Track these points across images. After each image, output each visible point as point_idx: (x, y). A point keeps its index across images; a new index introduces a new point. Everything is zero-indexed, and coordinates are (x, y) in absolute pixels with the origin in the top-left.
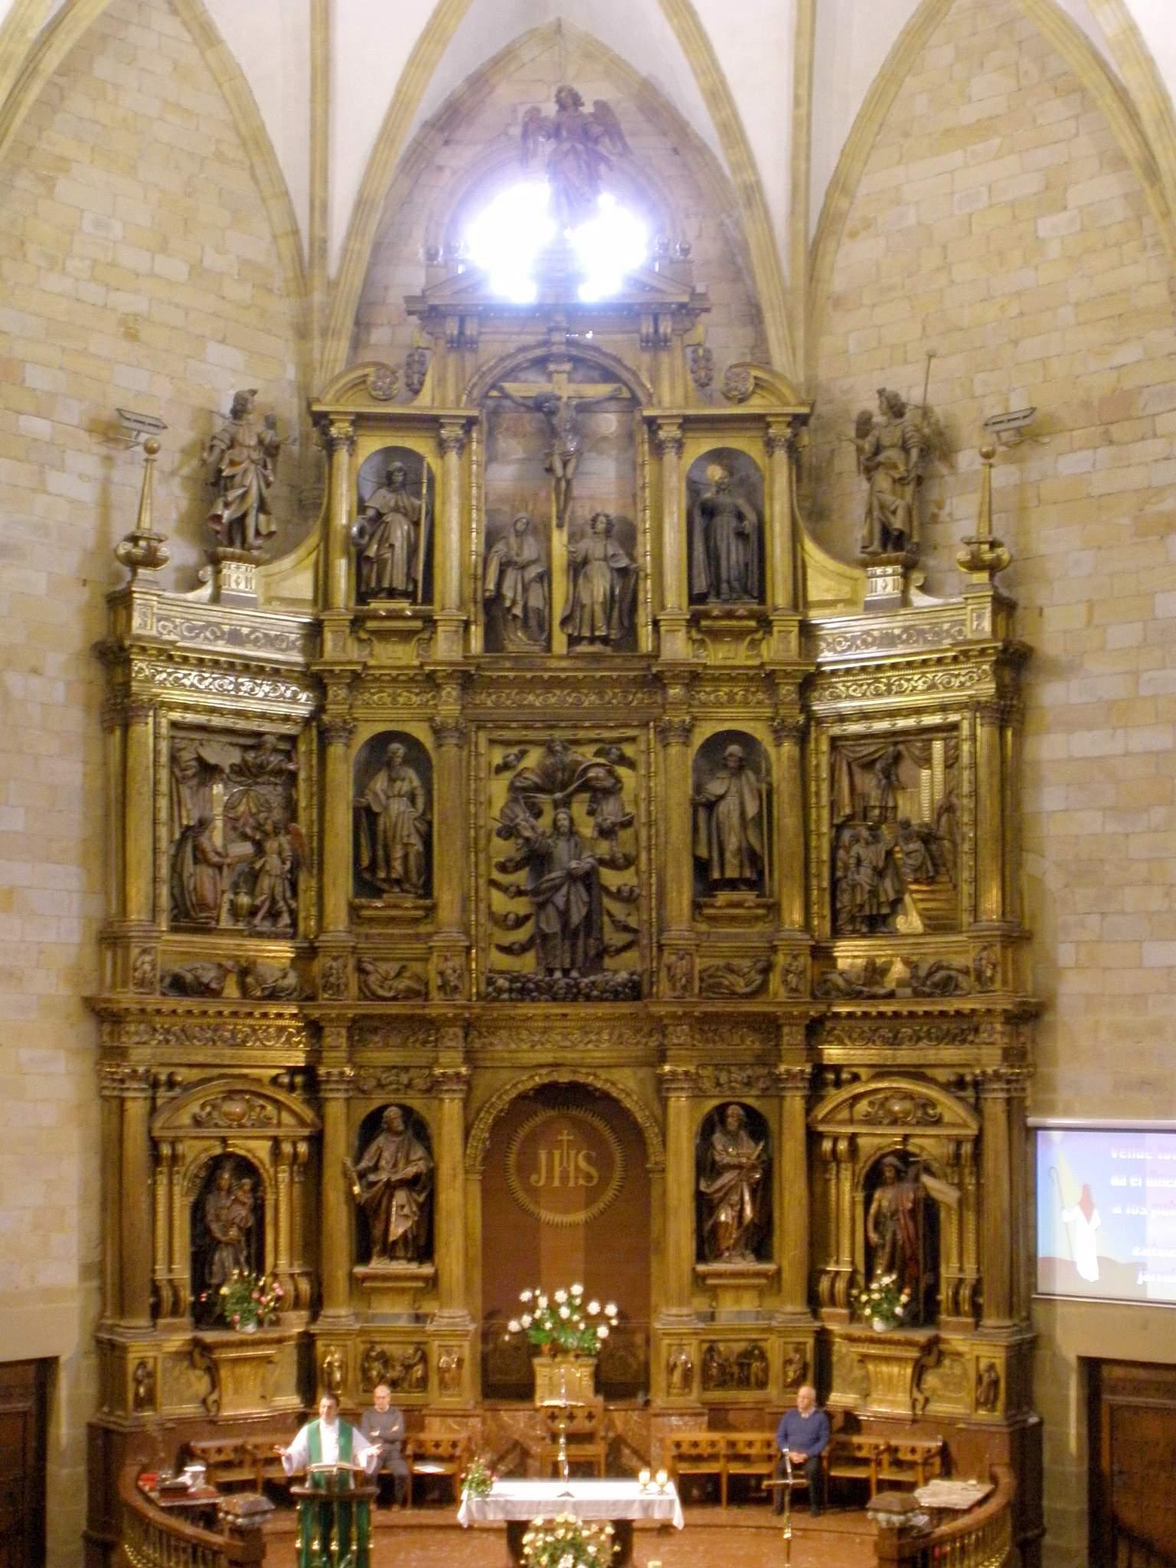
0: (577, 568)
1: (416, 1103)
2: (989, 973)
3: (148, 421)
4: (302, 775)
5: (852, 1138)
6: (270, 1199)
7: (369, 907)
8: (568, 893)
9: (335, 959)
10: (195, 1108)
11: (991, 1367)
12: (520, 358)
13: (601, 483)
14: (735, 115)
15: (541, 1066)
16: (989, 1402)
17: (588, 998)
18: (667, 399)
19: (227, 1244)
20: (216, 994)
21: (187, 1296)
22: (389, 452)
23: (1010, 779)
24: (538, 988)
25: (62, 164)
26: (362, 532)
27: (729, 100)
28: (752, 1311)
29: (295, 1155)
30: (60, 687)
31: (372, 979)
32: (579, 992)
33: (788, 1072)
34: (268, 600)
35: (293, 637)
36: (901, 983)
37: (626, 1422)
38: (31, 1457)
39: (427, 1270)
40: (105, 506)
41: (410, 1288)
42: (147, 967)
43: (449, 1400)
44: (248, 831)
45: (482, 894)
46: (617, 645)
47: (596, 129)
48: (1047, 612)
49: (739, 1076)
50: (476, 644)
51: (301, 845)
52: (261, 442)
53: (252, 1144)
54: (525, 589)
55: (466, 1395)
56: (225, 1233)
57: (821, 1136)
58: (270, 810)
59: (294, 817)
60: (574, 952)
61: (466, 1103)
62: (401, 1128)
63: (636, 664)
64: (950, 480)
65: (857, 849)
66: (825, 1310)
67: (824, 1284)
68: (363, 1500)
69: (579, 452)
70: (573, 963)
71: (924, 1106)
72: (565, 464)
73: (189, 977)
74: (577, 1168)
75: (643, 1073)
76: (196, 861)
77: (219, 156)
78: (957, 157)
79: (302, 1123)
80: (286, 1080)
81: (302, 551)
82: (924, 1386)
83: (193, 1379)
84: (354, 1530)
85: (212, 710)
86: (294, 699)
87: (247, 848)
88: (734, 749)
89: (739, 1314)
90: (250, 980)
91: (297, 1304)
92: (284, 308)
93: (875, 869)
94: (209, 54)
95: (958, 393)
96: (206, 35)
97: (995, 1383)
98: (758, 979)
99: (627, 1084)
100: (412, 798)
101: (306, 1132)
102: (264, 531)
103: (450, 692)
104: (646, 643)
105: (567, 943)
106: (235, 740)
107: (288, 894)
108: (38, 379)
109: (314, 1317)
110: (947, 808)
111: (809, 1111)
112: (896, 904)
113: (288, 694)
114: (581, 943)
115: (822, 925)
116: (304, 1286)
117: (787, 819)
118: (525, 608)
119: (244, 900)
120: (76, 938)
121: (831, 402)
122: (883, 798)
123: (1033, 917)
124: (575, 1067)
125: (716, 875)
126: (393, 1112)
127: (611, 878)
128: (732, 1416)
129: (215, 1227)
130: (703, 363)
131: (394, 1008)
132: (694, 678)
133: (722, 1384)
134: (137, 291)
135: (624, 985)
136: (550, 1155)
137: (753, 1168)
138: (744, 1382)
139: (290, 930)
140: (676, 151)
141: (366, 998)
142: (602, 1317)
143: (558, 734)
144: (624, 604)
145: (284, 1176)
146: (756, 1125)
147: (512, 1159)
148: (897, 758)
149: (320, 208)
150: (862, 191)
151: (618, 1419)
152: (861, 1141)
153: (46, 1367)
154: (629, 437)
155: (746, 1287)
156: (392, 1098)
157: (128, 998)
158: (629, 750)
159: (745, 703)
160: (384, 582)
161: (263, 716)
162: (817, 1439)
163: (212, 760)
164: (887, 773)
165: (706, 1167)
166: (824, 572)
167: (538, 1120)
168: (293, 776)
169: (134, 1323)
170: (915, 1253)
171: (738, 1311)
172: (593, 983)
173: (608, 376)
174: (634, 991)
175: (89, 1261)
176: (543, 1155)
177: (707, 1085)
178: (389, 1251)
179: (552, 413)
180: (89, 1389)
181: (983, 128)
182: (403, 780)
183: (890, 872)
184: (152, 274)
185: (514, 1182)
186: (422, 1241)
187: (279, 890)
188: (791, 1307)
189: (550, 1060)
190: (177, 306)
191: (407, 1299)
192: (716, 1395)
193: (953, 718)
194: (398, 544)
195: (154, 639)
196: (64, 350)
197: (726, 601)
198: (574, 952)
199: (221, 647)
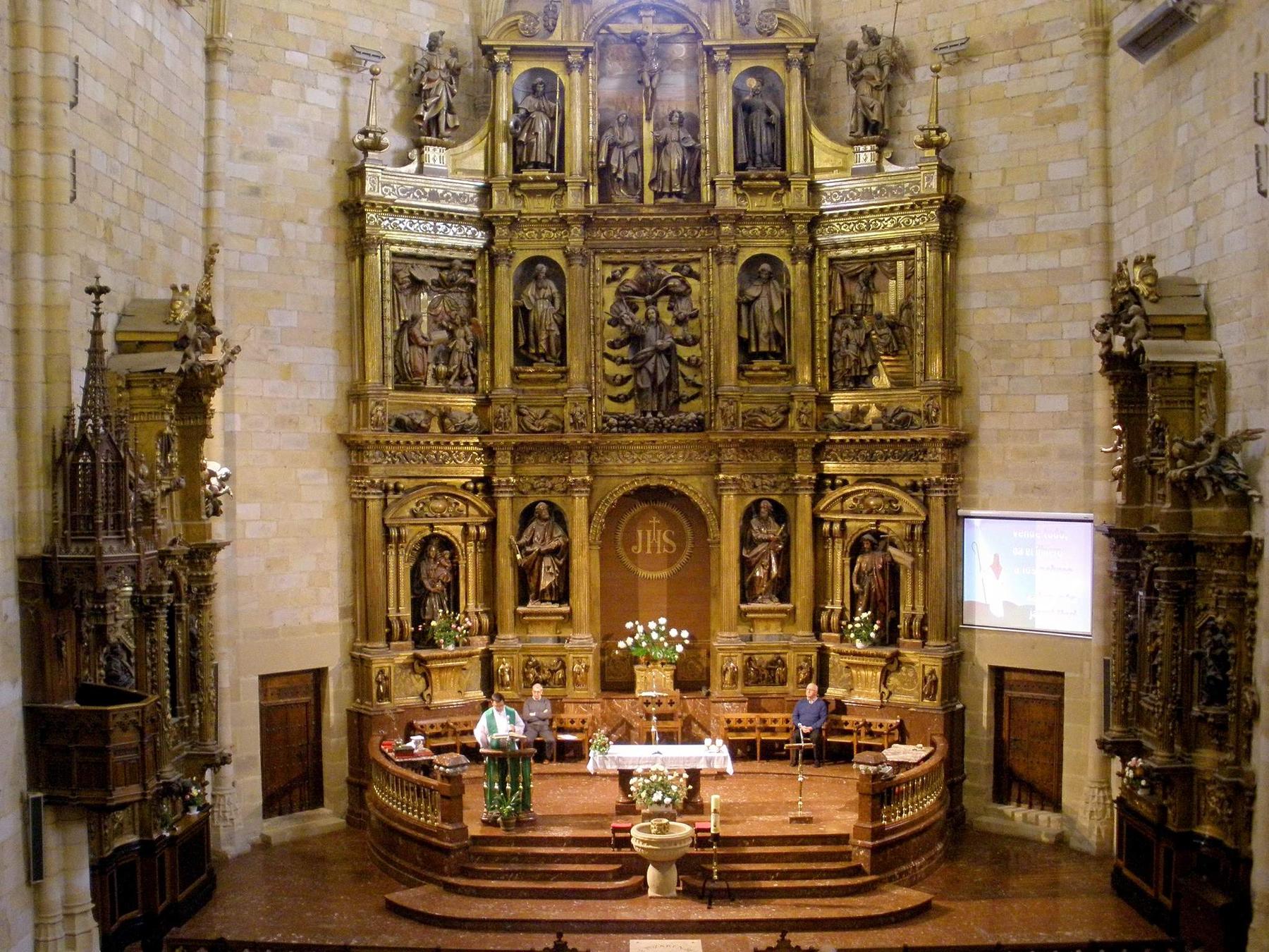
1: (557, 500)
6: (462, 563)
13: (675, 90)
15: (638, 475)
16: (930, 695)
17: (669, 430)
20: (425, 430)
22: (534, 72)
23: (948, 286)
24: (636, 424)
29: (478, 534)
30: (319, 231)
31: (526, 419)
35: (471, 195)
36: (875, 421)
37: (695, 707)
38: (312, 734)
39: (565, 609)
40: (345, 111)
42: (380, 414)
43: (580, 693)
50: (594, 198)
52: (448, 66)
53: (450, 528)
56: (434, 587)
57: (822, 521)
59: (474, 314)
60: (659, 400)
61: (590, 499)
67: (824, 617)
70: (659, 407)
72: (651, 80)
73: (407, 419)
75: (710, 478)
76: (411, 344)
79: (482, 514)
86: (473, 237)
90: (447, 421)
97: (935, 683)
98: (781, 418)
99: (695, 487)
101: (485, 520)
102: (451, 125)
103: (577, 229)
104: (706, 196)
106: (434, 263)
108: (296, 26)
109: (492, 641)
110: (907, 306)
113: (469, 233)
114: (664, 396)
115: (823, 383)
117: (800, 312)
118: (626, 175)
119: (442, 368)
120: (333, 396)
124: (660, 476)
125: (753, 349)
126: (542, 506)
132: (738, 219)
133: (757, 683)
135: (693, 421)
137: (777, 541)
138: (771, 681)
141: (523, 432)
142: (679, 639)
143: (648, 257)
146: (780, 514)
147: (620, 536)
152: (848, 524)
153: (319, 675)
154: (694, 60)
155: (773, 619)
156: (541, 497)
157: (368, 434)
159: (773, 236)
160: (531, 157)
162: (819, 718)
163: (420, 278)
165: (747, 541)
167: (638, 510)
168: (473, 287)
170: (883, 600)
171: (767, 636)
173: (680, 19)
174: (699, 425)
176: (640, 533)
178: (540, 597)
179: (642, 44)
180: (348, 688)
185: (621, 550)
191: (552, 628)
192: (754, 689)
195: (379, 198)
197: (759, 169)
198: (659, 400)
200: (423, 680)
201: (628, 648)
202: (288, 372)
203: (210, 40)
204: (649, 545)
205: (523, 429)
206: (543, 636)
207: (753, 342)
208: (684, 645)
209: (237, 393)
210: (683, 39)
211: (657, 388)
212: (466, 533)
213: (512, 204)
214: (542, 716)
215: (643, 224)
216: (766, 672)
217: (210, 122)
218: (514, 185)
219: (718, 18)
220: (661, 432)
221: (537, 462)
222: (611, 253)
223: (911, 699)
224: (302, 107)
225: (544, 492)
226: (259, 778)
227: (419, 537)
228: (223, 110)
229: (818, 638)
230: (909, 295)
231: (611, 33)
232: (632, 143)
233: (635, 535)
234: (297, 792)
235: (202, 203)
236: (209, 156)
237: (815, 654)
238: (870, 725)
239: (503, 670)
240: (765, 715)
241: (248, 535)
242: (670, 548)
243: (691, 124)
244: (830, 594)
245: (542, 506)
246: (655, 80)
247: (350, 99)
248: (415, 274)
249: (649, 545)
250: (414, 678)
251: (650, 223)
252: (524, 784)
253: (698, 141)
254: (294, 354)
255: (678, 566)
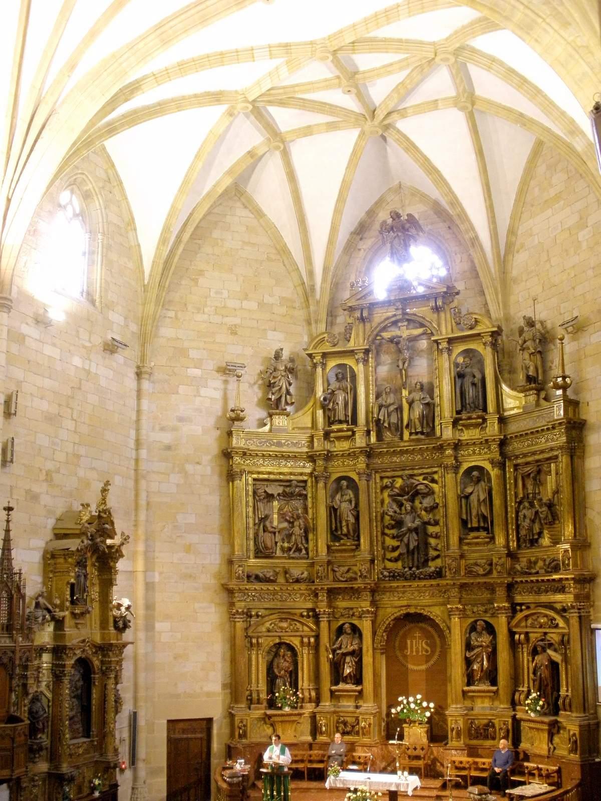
0: (411, 404)
1: (356, 622)
2: (567, 562)
3: (237, 365)
4: (309, 495)
5: (527, 634)
6: (299, 659)
7: (335, 546)
8: (409, 538)
9: (320, 566)
10: (267, 625)
11: (574, 735)
12: (387, 322)
13: (421, 370)
14: (463, 210)
15: (402, 606)
16: (573, 750)
17: (420, 579)
18: (444, 331)
19: (281, 677)
20: (274, 581)
21: (264, 696)
22: (340, 366)
23: (576, 478)
24: (399, 575)
25: (201, 273)
26: (325, 399)
27: (460, 205)
28: (489, 708)
29: (309, 642)
30: (209, 468)
31: (338, 574)
32: (416, 576)
33: (498, 606)
34: (296, 428)
35: (303, 442)
36: (541, 568)
37: (438, 752)
38: (204, 756)
39: (359, 688)
40: (225, 399)
41: (353, 695)
42: (240, 572)
43: (366, 740)
44: (288, 518)
45: (379, 538)
46: (428, 435)
47: (407, 225)
48: (590, 403)
49: (482, 608)
50: (373, 439)
51: (308, 522)
52: (286, 368)
53: (292, 638)
54: (389, 415)
55: (374, 737)
56: (280, 673)
57: (515, 633)
58: (298, 510)
59: (307, 513)
60: (413, 560)
61: (373, 622)
62: (349, 632)
63: (434, 441)
64: (555, 350)
65: (524, 511)
66: (518, 707)
67: (517, 697)
68: (285, 775)
69: (411, 358)
70: (413, 564)
71: (552, 620)
72: (404, 363)
73: (261, 575)
74: (422, 646)
75: (442, 608)
76: (264, 531)
77: (268, 259)
78: (549, 212)
79: (312, 630)
80: (305, 614)
81: (306, 408)
82: (554, 742)
83: (266, 728)
84: (282, 787)
85: (270, 473)
86: (304, 467)
87: (285, 525)
88: (475, 473)
89: (483, 708)
90: (287, 576)
91: (310, 701)
92: (300, 314)
93: (530, 520)
94: (261, 221)
95: (547, 313)
96: (259, 213)
97: (576, 742)
98: (488, 568)
99: (436, 612)
100: (350, 501)
101: (313, 634)
102: (289, 402)
103: (362, 459)
104: (438, 433)
105: (410, 557)
106: (282, 484)
107: (304, 542)
108: (193, 354)
109: (317, 705)
110: (556, 492)
111: (509, 623)
112: (540, 534)
113: (302, 464)
114: (416, 556)
115: (513, 545)
116: (313, 694)
117: (497, 501)
118: (389, 424)
119: (286, 545)
120: (218, 562)
121: (514, 323)
122: (534, 489)
123: (591, 537)
124: (416, 606)
125: (469, 526)
126: (347, 626)
127: (431, 529)
128: (480, 751)
129: (276, 671)
130: (458, 315)
131: (342, 585)
132: (457, 446)
133: (477, 738)
134: (236, 316)
135: (433, 573)
136: (412, 642)
137: (488, 646)
138: (486, 737)
139: (306, 556)
140: (449, 227)
141: (336, 581)
142: (428, 708)
143: (407, 472)
144: (429, 418)
145: (305, 651)
146: (490, 629)
147: (397, 644)
148: (539, 472)
149: (311, 273)
150: (519, 232)
151: (435, 750)
152: (531, 635)
153: (210, 721)
154: (430, 349)
155: (485, 697)
156: (346, 620)
157: (233, 585)
158: (436, 477)
159: (480, 454)
160: (337, 418)
161: (291, 474)
162: (507, 762)
163: (270, 492)
164: (535, 479)
165: (469, 647)
166: (510, 396)
167: (407, 627)
168: (306, 496)
169: (239, 706)
170: (549, 684)
171: (483, 708)
172: (421, 572)
173: (422, 325)
174: (439, 574)
175: (226, 682)
176: (409, 642)
177: (469, 613)
178: (345, 680)
179: (397, 343)
180: (226, 731)
181: (558, 197)
182: (346, 495)
183: (537, 521)
184: (241, 308)
185: (398, 653)
186: (358, 677)
187: (299, 540)
188: (502, 706)
189: (406, 604)
190: (253, 319)
191: (353, 700)
192: (474, 742)
193: (555, 453)
194: (340, 403)
195: (239, 448)
196: (205, 342)
197: (469, 412)
198: (413, 560)
199: (273, 448)
200: (271, 729)
201: (398, 713)
202: (188, 549)
203: (138, 367)
204: (414, 650)
205: (335, 580)
206: (348, 705)
207: (469, 521)
208: (431, 712)
209: (156, 560)
210: (425, 337)
211: (410, 553)
212: (302, 642)
213: (328, 446)
214: (339, 752)
215: (402, 452)
216: (482, 731)
217: (139, 412)
218: (327, 435)
219: (443, 323)
220: (414, 579)
221: (343, 599)
222: (385, 471)
223: (565, 753)
224: (198, 399)
225: (349, 617)
226: (165, 779)
227: (272, 644)
228: (145, 404)
229: (514, 710)
230: (558, 485)
231: (383, 339)
232: (393, 404)
233: (406, 643)
234: (192, 791)
235: (134, 457)
236: (138, 430)
237: (510, 720)
238: (541, 769)
239: (321, 724)
240: (477, 760)
241: (162, 640)
242: (427, 651)
243: (429, 389)
244: (521, 681)
245: (347, 626)
246: (406, 365)
247: (228, 392)
248: (267, 490)
249: (414, 650)
250: (265, 727)
251: (407, 452)
252: (284, 793)
253: (432, 398)
254: (194, 538)
255: (432, 662)
